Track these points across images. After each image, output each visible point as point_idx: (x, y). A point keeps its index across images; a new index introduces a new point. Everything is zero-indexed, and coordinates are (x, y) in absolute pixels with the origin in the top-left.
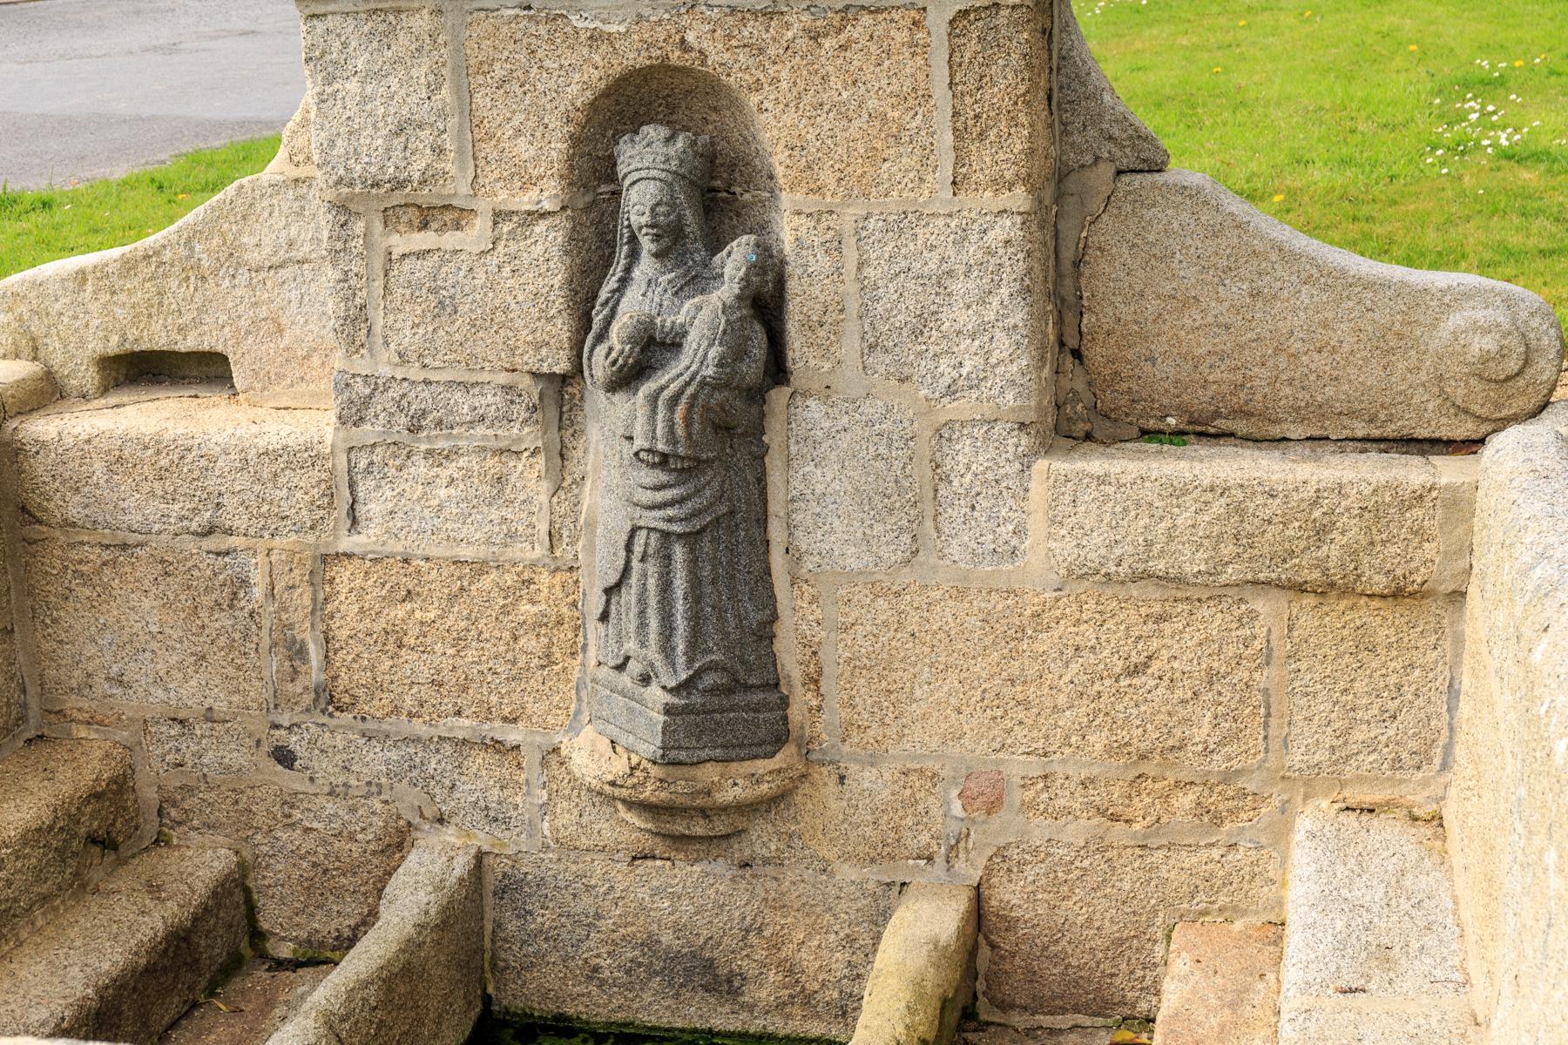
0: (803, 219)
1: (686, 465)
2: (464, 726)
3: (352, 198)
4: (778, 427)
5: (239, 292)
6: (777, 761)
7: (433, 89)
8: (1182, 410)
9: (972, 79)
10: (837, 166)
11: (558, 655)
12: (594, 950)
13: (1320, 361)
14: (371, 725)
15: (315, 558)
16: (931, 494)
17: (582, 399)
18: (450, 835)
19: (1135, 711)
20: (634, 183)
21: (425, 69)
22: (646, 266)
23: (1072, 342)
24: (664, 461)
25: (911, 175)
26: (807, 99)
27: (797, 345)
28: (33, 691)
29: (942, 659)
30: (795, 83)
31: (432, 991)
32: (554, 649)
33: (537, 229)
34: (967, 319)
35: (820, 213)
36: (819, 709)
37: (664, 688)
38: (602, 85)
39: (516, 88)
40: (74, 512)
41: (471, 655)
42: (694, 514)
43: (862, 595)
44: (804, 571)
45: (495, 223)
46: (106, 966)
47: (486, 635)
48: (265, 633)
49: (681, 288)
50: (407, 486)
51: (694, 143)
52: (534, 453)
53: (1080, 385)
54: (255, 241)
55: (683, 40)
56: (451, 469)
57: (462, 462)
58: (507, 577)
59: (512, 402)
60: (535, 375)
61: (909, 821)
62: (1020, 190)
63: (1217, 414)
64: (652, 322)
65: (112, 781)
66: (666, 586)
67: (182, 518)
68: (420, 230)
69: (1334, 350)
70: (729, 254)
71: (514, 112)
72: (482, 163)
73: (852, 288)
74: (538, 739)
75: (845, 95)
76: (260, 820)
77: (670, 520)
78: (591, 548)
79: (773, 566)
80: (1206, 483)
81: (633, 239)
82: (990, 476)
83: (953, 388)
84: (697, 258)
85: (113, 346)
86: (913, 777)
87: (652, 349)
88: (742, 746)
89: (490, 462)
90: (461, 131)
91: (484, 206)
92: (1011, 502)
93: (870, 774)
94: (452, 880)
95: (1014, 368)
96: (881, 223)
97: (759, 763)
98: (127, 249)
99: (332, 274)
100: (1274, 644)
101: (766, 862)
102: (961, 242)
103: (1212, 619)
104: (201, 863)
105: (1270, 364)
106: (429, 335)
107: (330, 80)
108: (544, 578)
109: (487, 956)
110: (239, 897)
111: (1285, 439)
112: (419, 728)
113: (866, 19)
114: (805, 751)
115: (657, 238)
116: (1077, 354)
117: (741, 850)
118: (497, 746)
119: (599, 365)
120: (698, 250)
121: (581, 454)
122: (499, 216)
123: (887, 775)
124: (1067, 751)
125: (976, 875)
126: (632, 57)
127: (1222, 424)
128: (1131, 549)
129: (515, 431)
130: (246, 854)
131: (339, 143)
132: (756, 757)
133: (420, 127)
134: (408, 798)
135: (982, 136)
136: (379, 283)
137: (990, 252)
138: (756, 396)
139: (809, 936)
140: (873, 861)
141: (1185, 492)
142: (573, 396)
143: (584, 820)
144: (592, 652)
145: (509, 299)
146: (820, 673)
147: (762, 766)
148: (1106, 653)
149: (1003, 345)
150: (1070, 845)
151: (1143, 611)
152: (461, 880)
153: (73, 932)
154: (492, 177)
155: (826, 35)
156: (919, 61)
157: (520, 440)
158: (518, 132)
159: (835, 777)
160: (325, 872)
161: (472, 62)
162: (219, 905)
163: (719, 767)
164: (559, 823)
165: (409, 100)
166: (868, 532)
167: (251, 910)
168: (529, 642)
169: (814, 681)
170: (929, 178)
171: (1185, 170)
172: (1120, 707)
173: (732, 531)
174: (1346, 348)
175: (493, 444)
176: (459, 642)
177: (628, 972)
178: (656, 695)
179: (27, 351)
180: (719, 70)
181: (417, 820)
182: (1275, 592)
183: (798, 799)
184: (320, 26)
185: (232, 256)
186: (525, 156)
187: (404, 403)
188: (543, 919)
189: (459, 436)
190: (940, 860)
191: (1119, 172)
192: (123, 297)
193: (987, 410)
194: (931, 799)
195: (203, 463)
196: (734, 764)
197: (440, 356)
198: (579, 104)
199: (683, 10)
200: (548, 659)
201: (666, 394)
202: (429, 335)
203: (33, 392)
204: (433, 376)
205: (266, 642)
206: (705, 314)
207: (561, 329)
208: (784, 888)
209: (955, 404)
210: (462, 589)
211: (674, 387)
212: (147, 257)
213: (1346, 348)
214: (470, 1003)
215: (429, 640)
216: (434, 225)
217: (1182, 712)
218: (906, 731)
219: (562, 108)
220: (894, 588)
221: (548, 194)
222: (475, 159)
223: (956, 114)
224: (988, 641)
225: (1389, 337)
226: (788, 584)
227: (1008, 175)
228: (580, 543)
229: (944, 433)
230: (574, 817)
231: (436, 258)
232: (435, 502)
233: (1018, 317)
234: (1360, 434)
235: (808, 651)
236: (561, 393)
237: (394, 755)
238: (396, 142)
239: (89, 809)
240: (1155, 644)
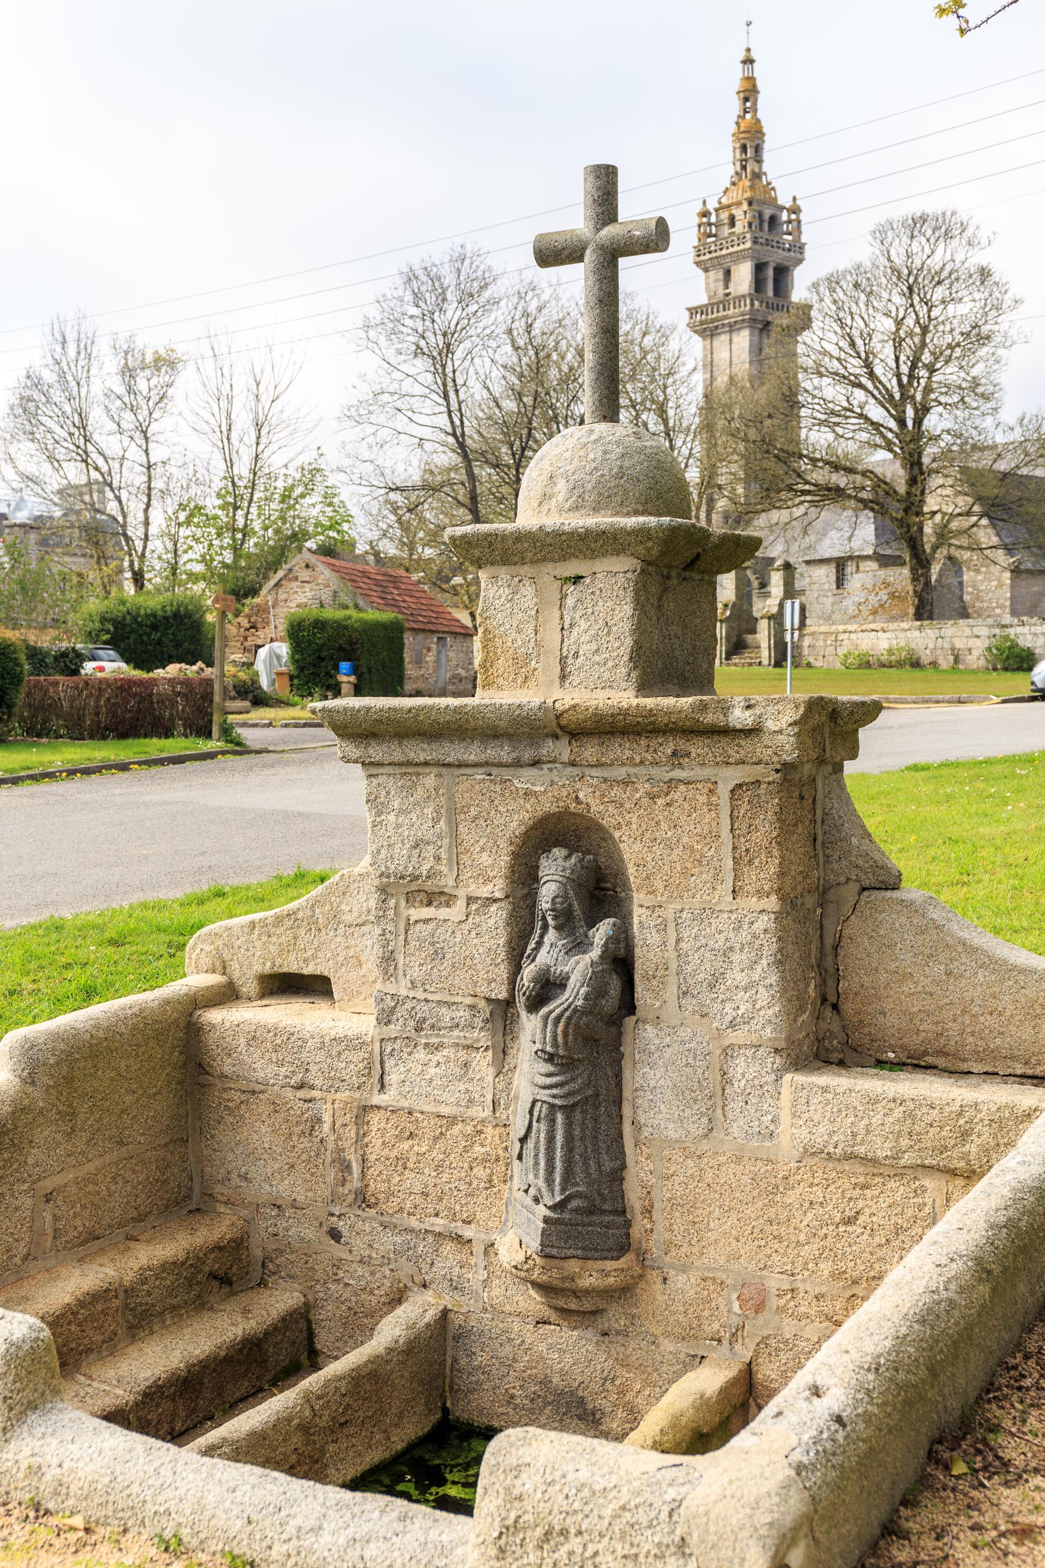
0: (644, 910)
2: (439, 1224)
3: (388, 885)
5: (338, 939)
6: (621, 1263)
7: (436, 821)
8: (904, 1048)
9: (744, 826)
12: (511, 1383)
13: (991, 1021)
14: (386, 1218)
15: (359, 1107)
18: (429, 1296)
19: (848, 1250)
22: (551, 935)
23: (833, 999)
24: (550, 1058)
26: (648, 835)
28: (197, 1180)
31: (396, 1393)
34: (741, 979)
35: (654, 907)
36: (652, 1230)
38: (531, 822)
40: (227, 1069)
41: (445, 1177)
43: (677, 1156)
46: (197, 1352)
48: (328, 1153)
50: (412, 1065)
52: (487, 1049)
53: (836, 1027)
54: (348, 908)
55: (577, 797)
56: (438, 1056)
57: (445, 1052)
60: (488, 1000)
61: (706, 1313)
62: (773, 898)
63: (925, 1053)
64: (548, 970)
65: (231, 1240)
66: (551, 1139)
67: (286, 1077)
69: (1000, 1014)
72: (461, 867)
73: (673, 955)
74: (483, 1236)
76: (320, 1275)
77: (554, 1096)
78: (515, 1112)
80: (890, 1096)
81: (544, 918)
82: (756, 1082)
85: (267, 969)
86: (709, 1283)
88: (596, 1250)
89: (460, 1053)
90: (450, 847)
92: (770, 1101)
93: (682, 1278)
94: (421, 1324)
95: (771, 1012)
98: (277, 910)
99: (378, 931)
100: (937, 1210)
101: (618, 1333)
102: (738, 929)
103: (898, 1190)
104: (278, 1301)
105: (959, 1020)
107: (379, 814)
108: (489, 1130)
109: (447, 1381)
110: (303, 1324)
111: (970, 1073)
112: (413, 1222)
113: (682, 788)
114: (642, 1256)
115: (555, 918)
116: (835, 1007)
117: (603, 1323)
118: (458, 1238)
122: (470, 900)
123: (693, 1280)
124: (806, 1273)
125: (748, 1355)
126: (548, 806)
127: (930, 1060)
128: (842, 1137)
130: (310, 1297)
131: (383, 851)
132: (605, 1259)
134: (405, 1269)
135: (750, 862)
136: (402, 938)
137: (755, 936)
139: (643, 1388)
140: (683, 1339)
141: (877, 1102)
143: (509, 1293)
144: (516, 1180)
146: (652, 1207)
147: (609, 1265)
148: (830, 1207)
149: (763, 996)
150: (808, 1340)
151: (853, 1180)
152: (428, 1325)
153: (185, 1331)
157: (478, 1040)
158: (483, 849)
159: (660, 1279)
160: (355, 1313)
162: (286, 1328)
163: (580, 1263)
164: (493, 1294)
167: (311, 1336)
168: (480, 1172)
169: (648, 1211)
171: (911, 890)
172: (839, 1246)
173: (596, 1107)
174: (1008, 1013)
175: (463, 1042)
177: (532, 1401)
178: (542, 1211)
179: (220, 969)
181: (410, 1284)
182: (937, 1174)
183: (638, 1291)
184: (375, 781)
185: (335, 916)
188: (482, 1359)
189: (444, 1036)
190: (725, 1342)
191: (864, 889)
192: (274, 939)
193: (754, 1038)
194: (720, 1299)
195: (300, 1043)
201: (553, 1015)
203: (217, 994)
204: (430, 997)
205: (329, 1159)
207: (503, 972)
208: (628, 1352)
211: (558, 1011)
212: (289, 915)
213: (1008, 1013)
214: (430, 1410)
217: (880, 1253)
221: (497, 888)
223: (734, 848)
224: (755, 1193)
225: (1036, 1006)
227: (766, 888)
229: (728, 1052)
230: (503, 1291)
232: (428, 1077)
233: (773, 979)
234: (1019, 1072)
235: (645, 1191)
237: (398, 1239)
239: (213, 1256)
240: (861, 1204)
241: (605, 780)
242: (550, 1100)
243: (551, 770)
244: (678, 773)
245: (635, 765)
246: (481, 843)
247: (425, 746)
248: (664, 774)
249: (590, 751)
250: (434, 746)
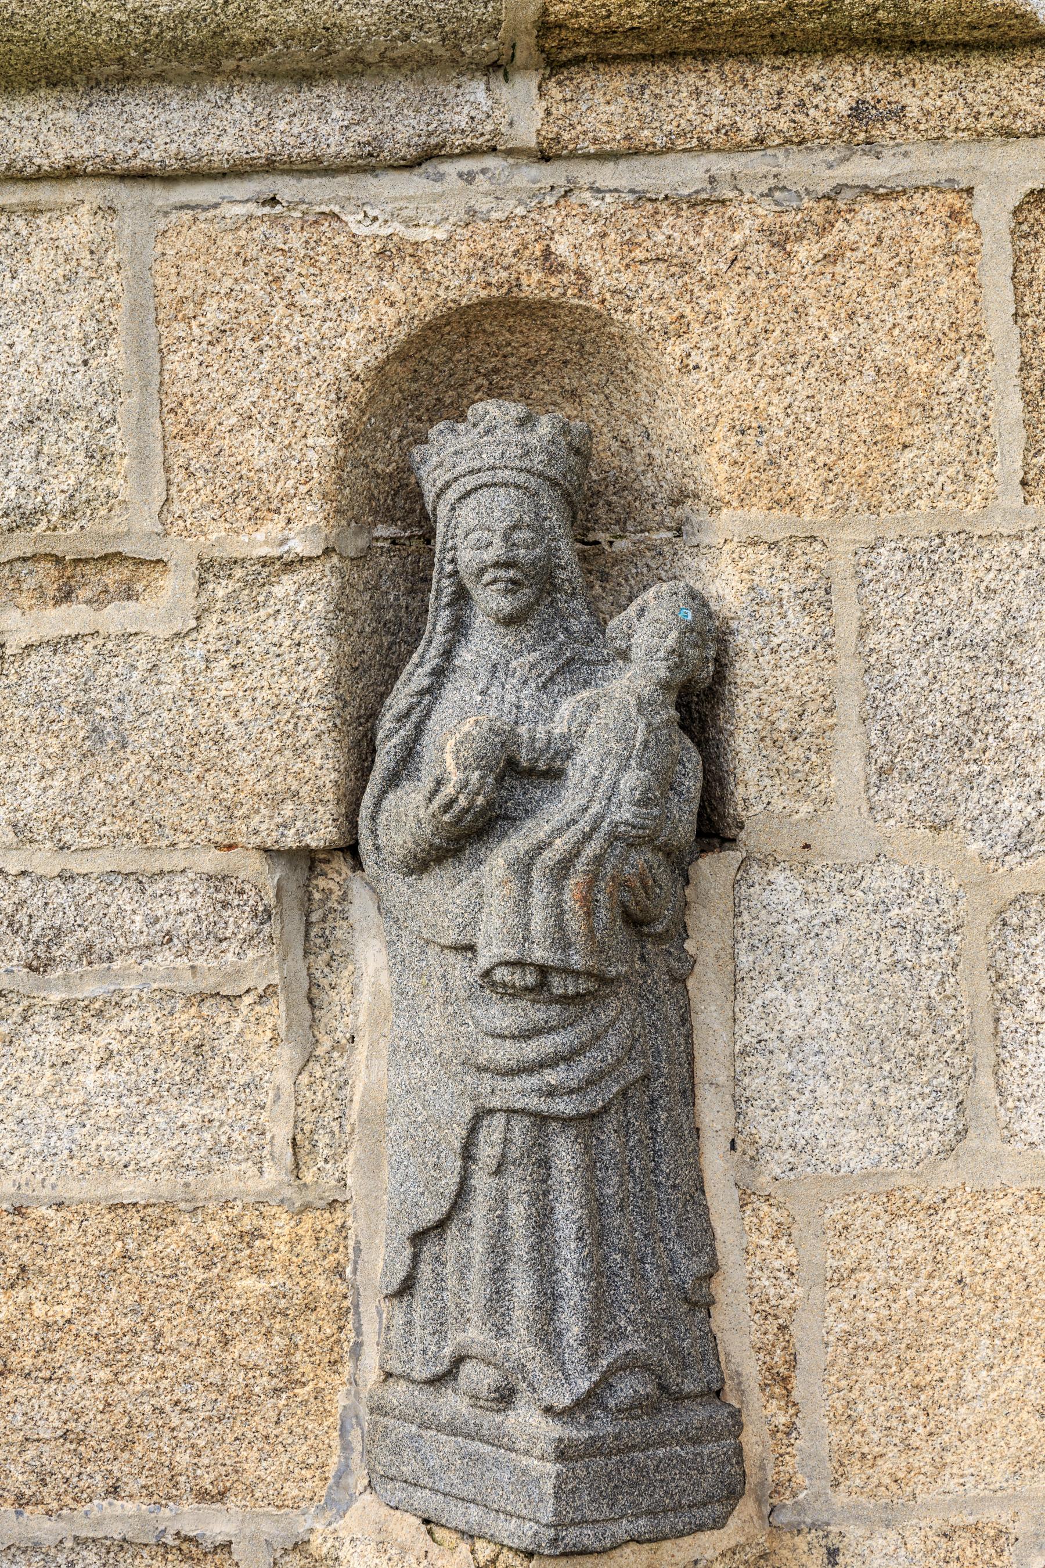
1: (582, 988)
4: (715, 922)
10: (821, 460)
11: (307, 1368)
16: (990, 1028)
17: (344, 898)
20: (468, 494)
21: (78, 312)
25: (951, 471)
26: (767, 347)
27: (751, 775)
29: (1013, 1321)
30: (747, 321)
32: (298, 1357)
33: (278, 591)
36: (791, 1428)
37: (548, 1410)
38: (401, 334)
39: (245, 342)
42: (593, 1081)
43: (867, 1216)
44: (765, 1179)
45: (202, 583)
47: (170, 1340)
49: (551, 679)
50: (22, 1071)
51: (566, 430)
55: (547, 253)
56: (107, 1035)
58: (212, 1228)
59: (225, 905)
66: (542, 1220)
68: (57, 602)
70: (641, 613)
71: (240, 385)
73: (849, 668)
74: (268, 1528)
75: (834, 337)
77: (551, 1093)
79: (708, 1175)
81: (461, 597)
83: (1026, 837)
84: (575, 626)
86: (961, 1541)
87: (518, 775)
90: (142, 419)
91: (180, 551)
96: (899, 555)
97: (705, 1538)
106: (73, 791)
108: (282, 1225)
113: (870, 210)
119: (404, 817)
120: (575, 614)
121: (345, 996)
122: (208, 568)
123: (914, 1542)
129: (230, 957)
132: (701, 1528)
133: (65, 414)
138: (680, 865)
142: (328, 893)
145: (226, 717)
146: (793, 1363)
154: (197, 501)
155: (800, 239)
156: (962, 277)
157: (239, 973)
159: (819, 1554)
161: (166, 298)
165: (47, 367)
166: (880, 1100)
168: (250, 1348)
169: (780, 1381)
170: (981, 475)
175: (187, 983)
176: (119, 1356)
180: (611, 302)
186: (259, 463)
187: (21, 917)
196: (667, 1545)
197: (92, 826)
198: (358, 367)
199: (549, 200)
200: (287, 1379)
201: (549, 857)
202: (73, 791)
204: (76, 864)
206: (607, 714)
207: (324, 765)
209: (1029, 864)
210: (125, 1256)
215: (60, 1356)
216: (84, 594)
218: (949, 1458)
219: (329, 376)
220: (926, 1201)
222: (167, 469)
226: (735, 1206)
228: (351, 1157)
231: (88, 649)
232: (76, 1098)
235: (772, 1326)
236: (306, 888)
238: (20, 443)
241: (640, 197)
242: (535, 1103)
243: (468, 178)
244: (863, 169)
245: (741, 148)
246: (243, 402)
247: (70, 118)
248: (814, 170)
249: (603, 107)
250: (98, 116)
